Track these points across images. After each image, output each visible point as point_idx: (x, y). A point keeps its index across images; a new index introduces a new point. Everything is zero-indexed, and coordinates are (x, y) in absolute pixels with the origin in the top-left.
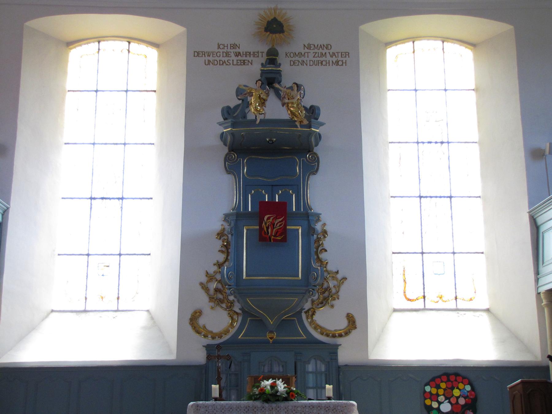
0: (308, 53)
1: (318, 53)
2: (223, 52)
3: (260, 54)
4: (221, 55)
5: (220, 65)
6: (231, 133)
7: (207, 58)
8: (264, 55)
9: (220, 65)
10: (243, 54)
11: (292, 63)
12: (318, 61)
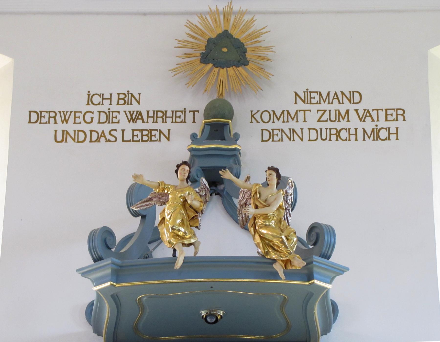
0: (304, 111)
1: (330, 111)
2: (100, 112)
3: (189, 117)
4: (96, 120)
5: (91, 141)
6: (112, 296)
7: (60, 127)
8: (200, 117)
9: (91, 141)
10: (148, 117)
11: (266, 135)
12: (328, 131)
